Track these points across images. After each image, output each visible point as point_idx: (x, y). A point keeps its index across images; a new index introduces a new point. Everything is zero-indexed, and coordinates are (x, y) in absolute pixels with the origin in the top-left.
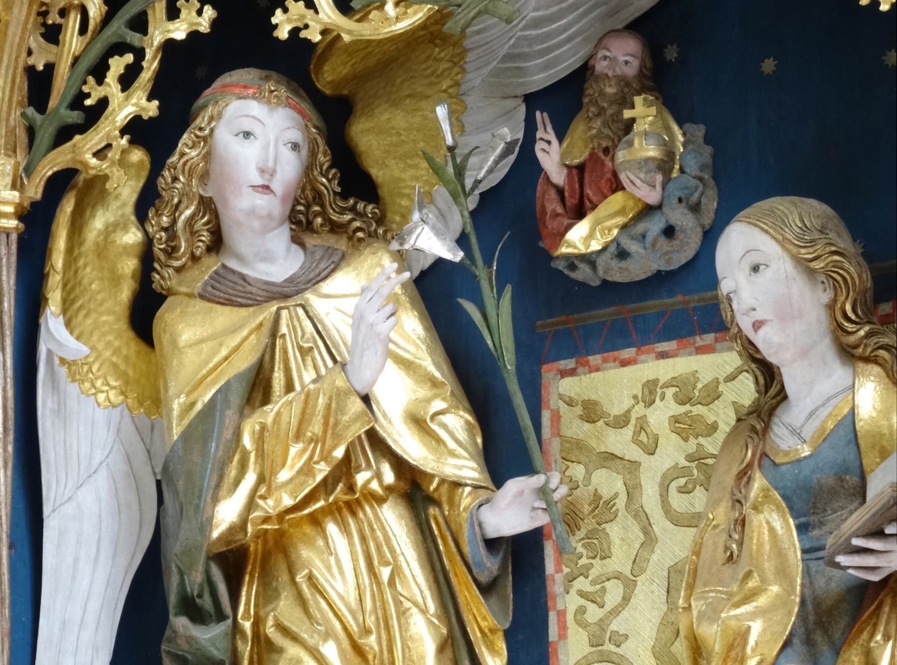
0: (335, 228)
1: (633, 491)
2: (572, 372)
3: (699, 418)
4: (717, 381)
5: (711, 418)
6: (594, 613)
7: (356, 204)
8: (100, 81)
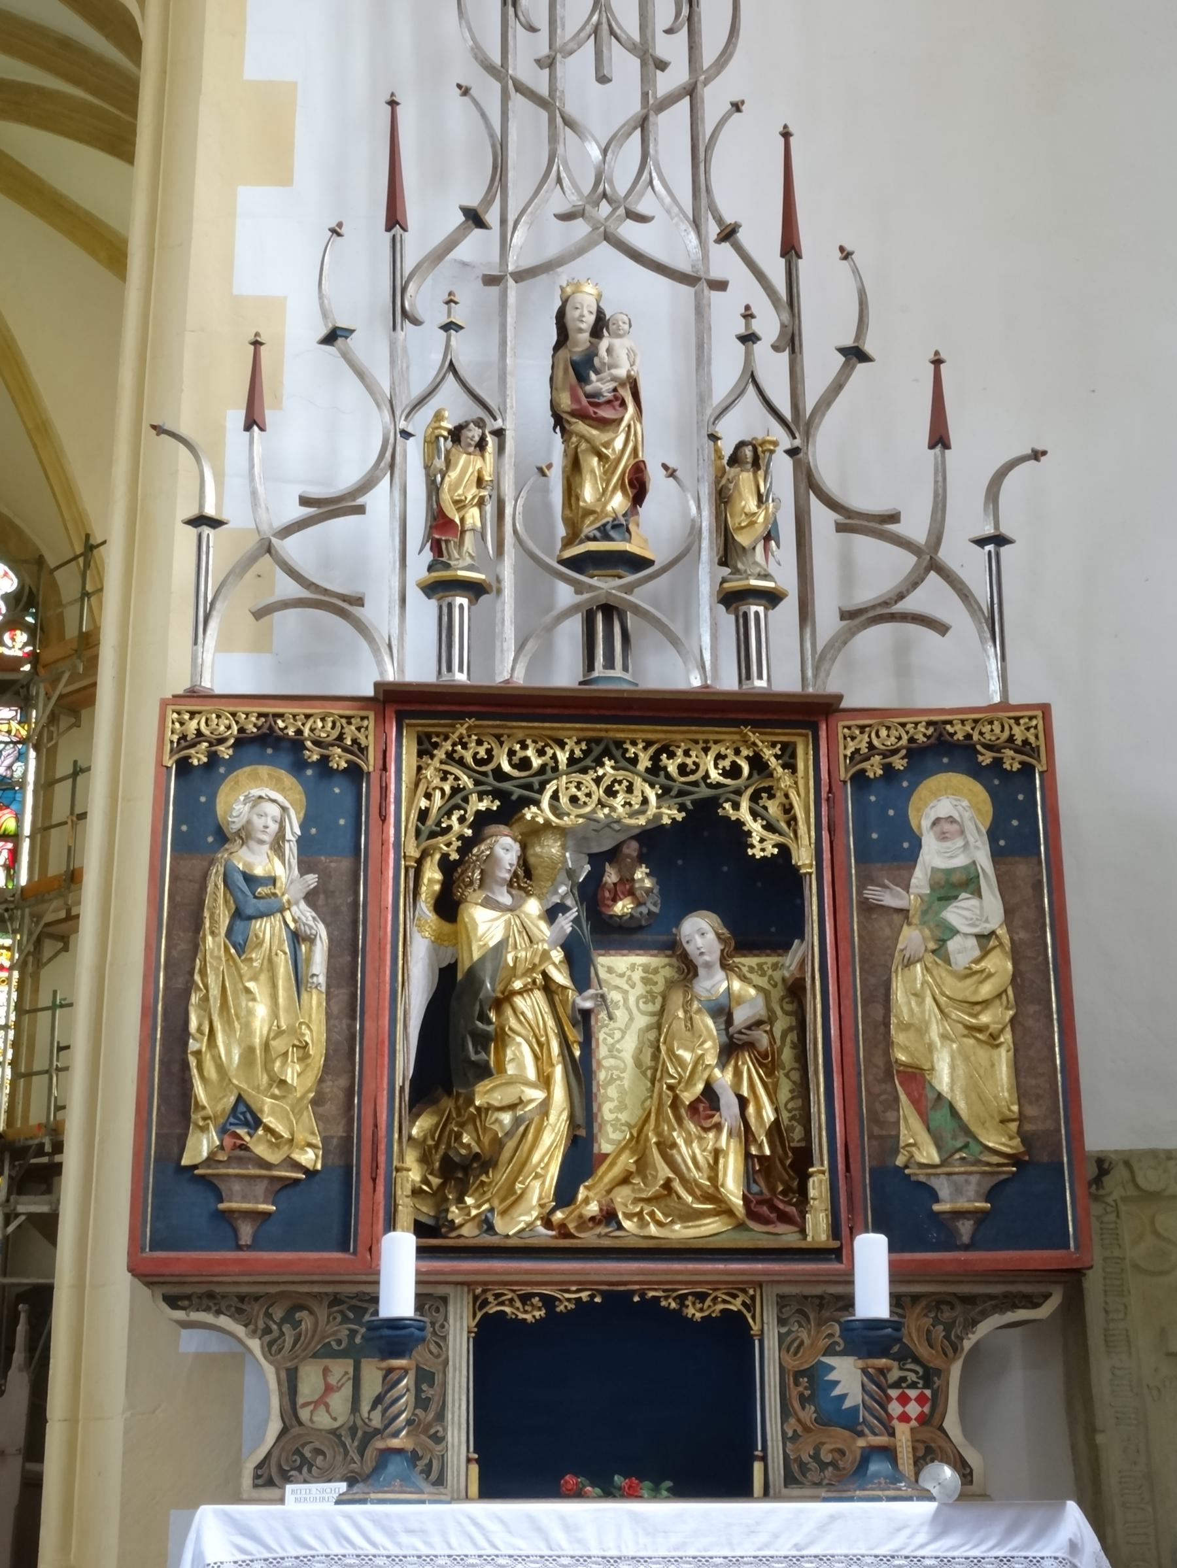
0: (520, 888)
1: (626, 1000)
2: (603, 955)
3: (651, 979)
4: (657, 968)
5: (655, 980)
6: (610, 1041)
7: (608, 899)
8: (449, 818)
